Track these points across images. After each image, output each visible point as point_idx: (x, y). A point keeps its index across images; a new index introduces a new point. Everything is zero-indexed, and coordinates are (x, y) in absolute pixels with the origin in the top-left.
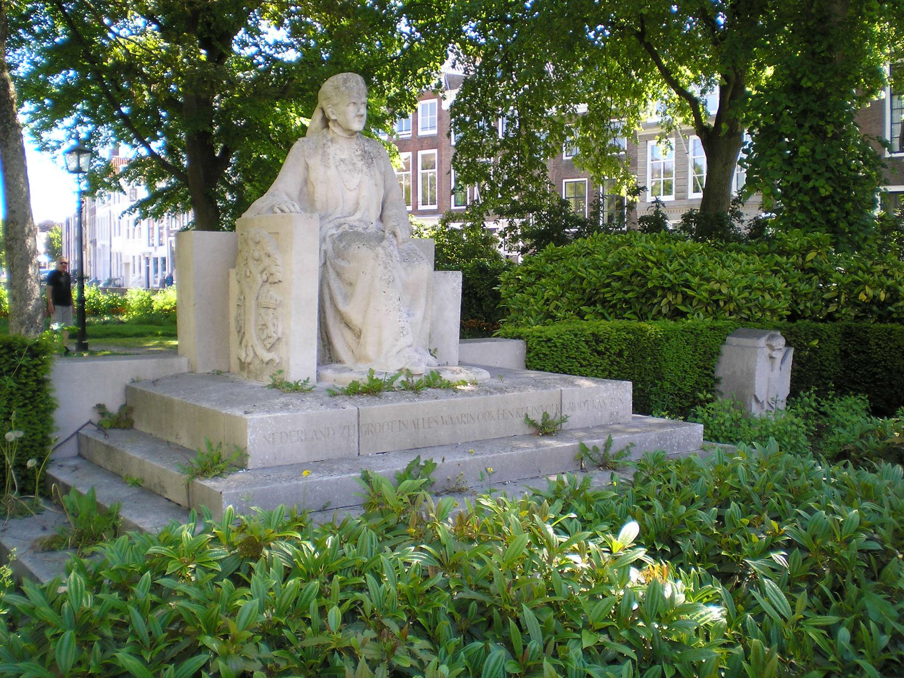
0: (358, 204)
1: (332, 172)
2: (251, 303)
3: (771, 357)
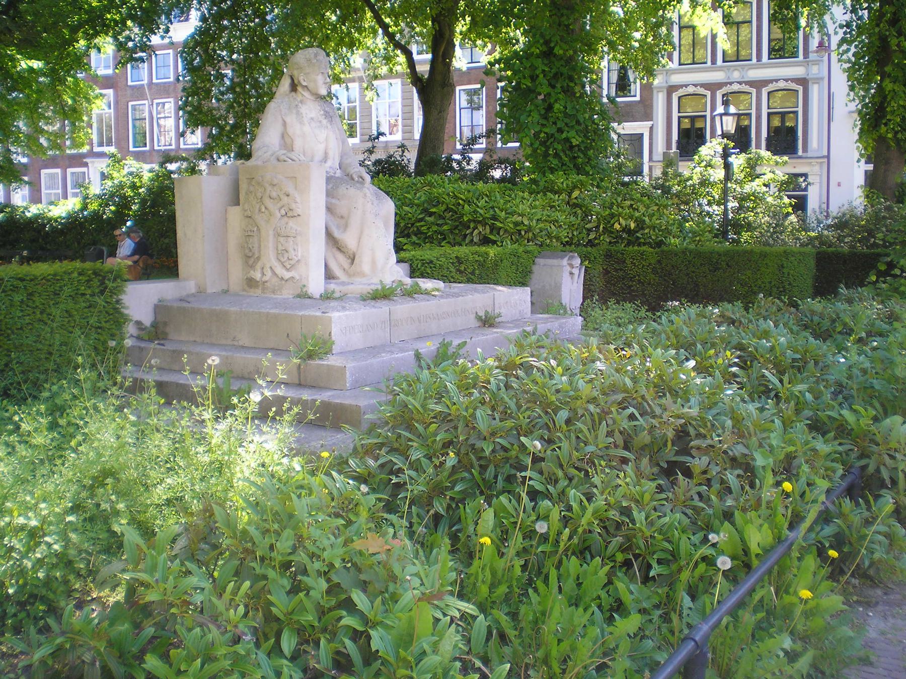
0: (326, 153)
1: (307, 129)
2: (268, 235)
3: (571, 273)
